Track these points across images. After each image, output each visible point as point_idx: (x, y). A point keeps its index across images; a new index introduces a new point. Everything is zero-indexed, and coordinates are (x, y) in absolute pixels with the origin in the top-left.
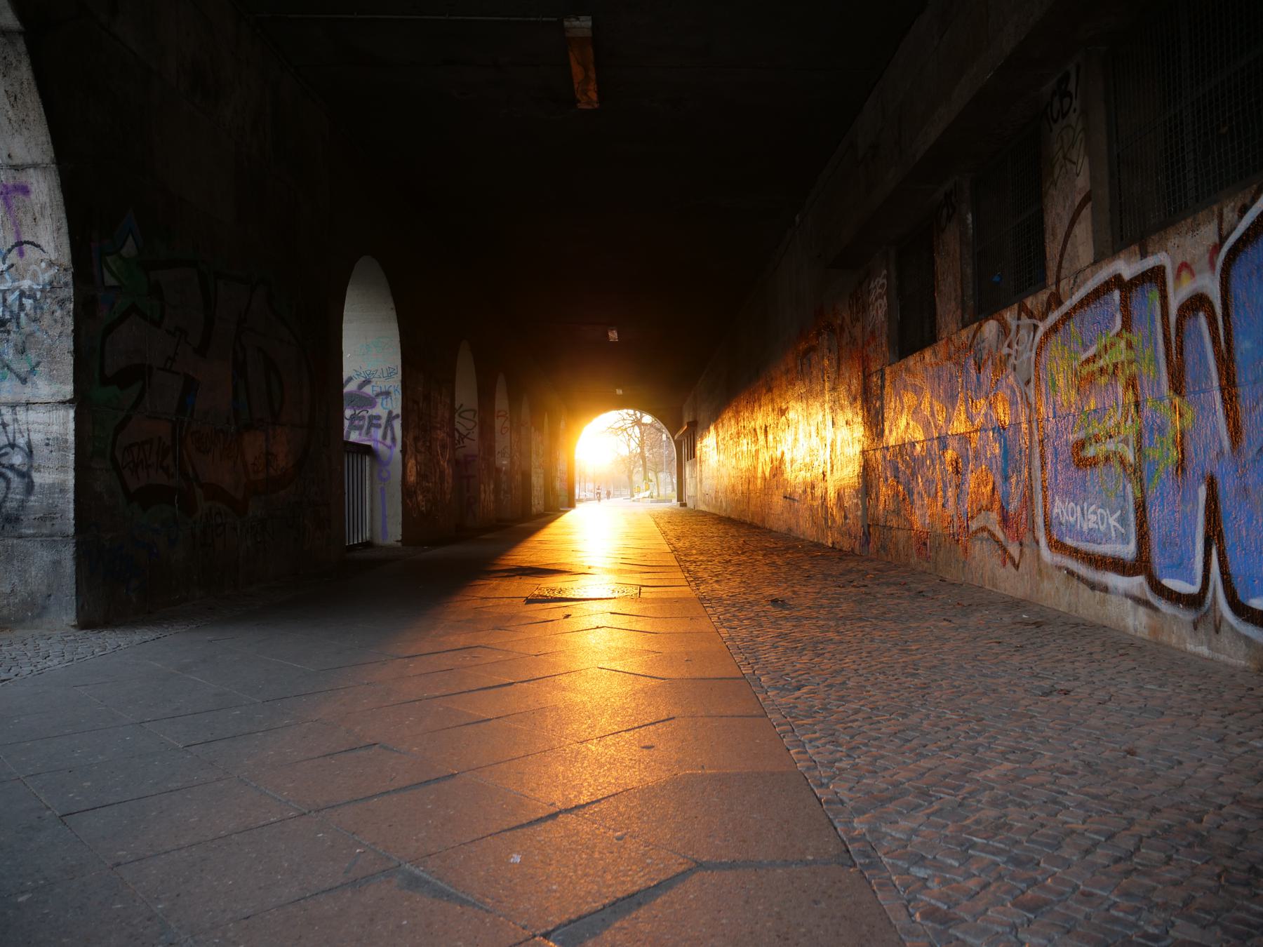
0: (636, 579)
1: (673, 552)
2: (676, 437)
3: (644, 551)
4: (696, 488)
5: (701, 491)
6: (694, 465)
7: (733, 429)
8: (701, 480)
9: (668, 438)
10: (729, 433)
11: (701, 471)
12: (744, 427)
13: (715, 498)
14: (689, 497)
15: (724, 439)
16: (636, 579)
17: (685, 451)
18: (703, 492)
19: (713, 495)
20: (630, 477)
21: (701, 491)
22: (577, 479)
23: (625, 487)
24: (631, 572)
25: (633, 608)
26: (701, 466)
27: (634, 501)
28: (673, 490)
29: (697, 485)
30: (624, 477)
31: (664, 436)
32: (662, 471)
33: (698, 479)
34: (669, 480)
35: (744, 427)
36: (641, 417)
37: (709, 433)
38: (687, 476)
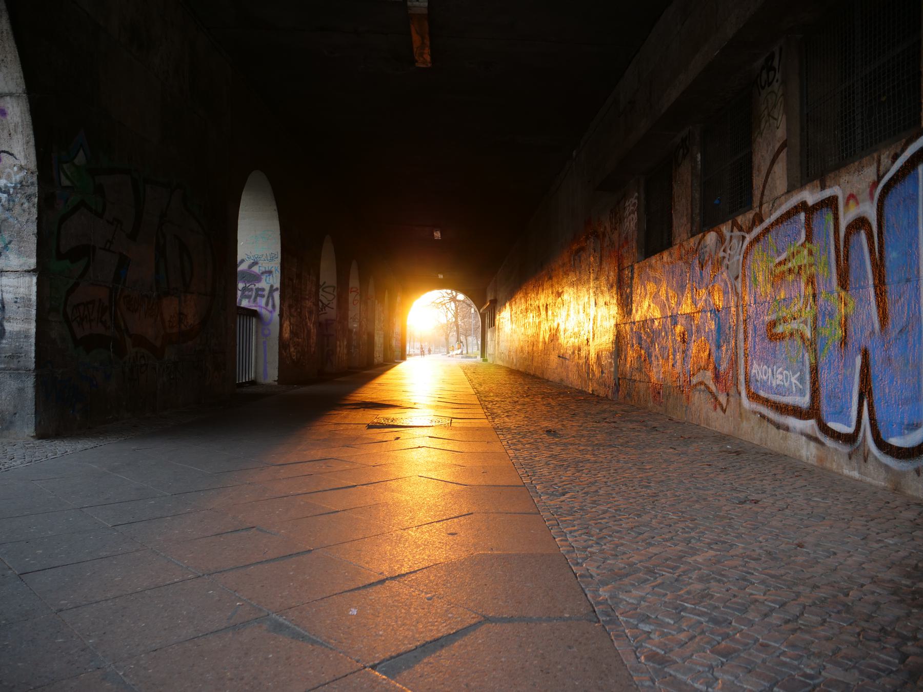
0: (449, 413)
1: (476, 394)
2: (481, 311)
3: (455, 393)
4: (495, 348)
5: (498, 350)
6: (494, 331)
7: (523, 306)
8: (498, 343)
9: (475, 311)
10: (520, 309)
11: (499, 336)
12: (531, 305)
13: (508, 356)
14: (489, 354)
15: (516, 313)
16: (449, 413)
17: (487, 321)
18: (500, 351)
19: (507, 354)
20: (447, 339)
21: (498, 350)
22: (408, 339)
23: (443, 346)
24: (445, 407)
25: (446, 434)
26: (499, 332)
27: (449, 356)
28: (478, 350)
29: (495, 346)
30: (443, 339)
31: (473, 310)
32: (470, 335)
33: (496, 342)
34: (475, 342)
35: (531, 305)
36: (456, 295)
37: (506, 308)
38: (489, 339)
